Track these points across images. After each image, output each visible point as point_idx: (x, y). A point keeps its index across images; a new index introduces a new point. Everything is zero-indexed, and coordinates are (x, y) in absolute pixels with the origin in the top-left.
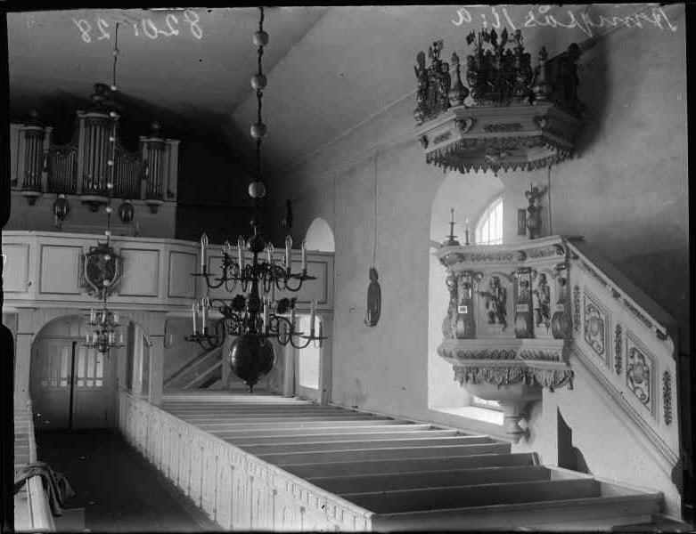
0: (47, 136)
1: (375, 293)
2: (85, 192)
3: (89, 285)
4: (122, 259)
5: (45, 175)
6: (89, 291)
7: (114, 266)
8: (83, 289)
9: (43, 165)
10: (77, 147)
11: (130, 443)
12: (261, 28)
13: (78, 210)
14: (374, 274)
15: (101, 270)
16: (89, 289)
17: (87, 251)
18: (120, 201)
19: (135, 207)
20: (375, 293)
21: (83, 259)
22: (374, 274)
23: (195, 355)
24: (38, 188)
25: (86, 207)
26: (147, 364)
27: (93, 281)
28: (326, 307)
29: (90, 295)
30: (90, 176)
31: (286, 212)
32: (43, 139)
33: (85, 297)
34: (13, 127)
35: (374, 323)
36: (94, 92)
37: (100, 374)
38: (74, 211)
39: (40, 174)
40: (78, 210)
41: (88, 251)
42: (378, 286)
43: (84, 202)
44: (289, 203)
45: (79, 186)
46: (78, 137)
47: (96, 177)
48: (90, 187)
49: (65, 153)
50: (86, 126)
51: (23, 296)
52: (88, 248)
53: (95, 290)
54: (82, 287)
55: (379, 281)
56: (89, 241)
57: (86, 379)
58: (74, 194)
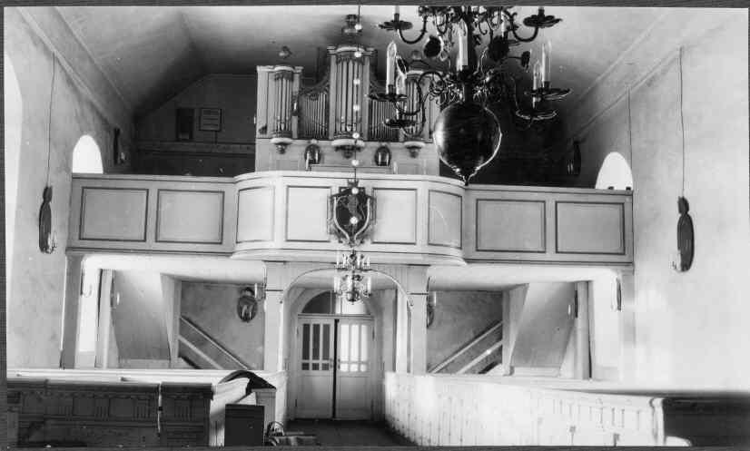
0: (297, 77)
1: (686, 229)
2: (337, 135)
3: (339, 231)
4: (373, 200)
5: (295, 120)
6: (339, 237)
7: (366, 207)
8: (333, 236)
9: (293, 108)
10: (329, 86)
11: (404, 435)
12: (573, 435)
13: (331, 156)
14: (684, 205)
15: (352, 212)
16: (339, 235)
17: (336, 191)
18: (376, 145)
19: (393, 152)
20: (686, 229)
21: (332, 201)
22: (684, 205)
23: (472, 336)
24: (289, 135)
25: (340, 153)
26: (410, 331)
27: (343, 228)
28: (624, 259)
29: (340, 242)
30: (343, 118)
31: (573, 153)
32: (292, 79)
33: (334, 244)
34: (260, 69)
35: (687, 263)
36: (345, 24)
37: (364, 358)
38: (327, 158)
39: (290, 119)
40: (331, 156)
41: (337, 192)
42: (690, 218)
43: (338, 148)
44: (576, 143)
45: (332, 128)
46: (329, 77)
47: (349, 118)
48: (343, 129)
49: (315, 97)
50: (337, 63)
51: (267, 245)
52: (338, 189)
53: (344, 237)
54: (331, 233)
55: (689, 213)
56: (335, 180)
57: (349, 363)
58: (327, 139)
